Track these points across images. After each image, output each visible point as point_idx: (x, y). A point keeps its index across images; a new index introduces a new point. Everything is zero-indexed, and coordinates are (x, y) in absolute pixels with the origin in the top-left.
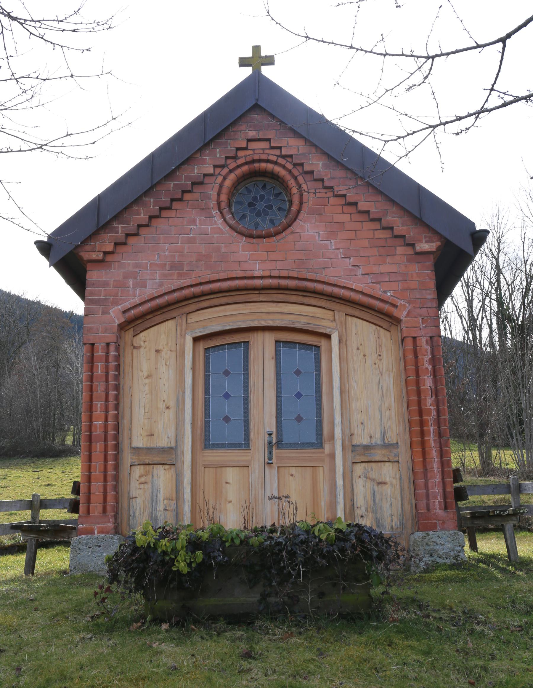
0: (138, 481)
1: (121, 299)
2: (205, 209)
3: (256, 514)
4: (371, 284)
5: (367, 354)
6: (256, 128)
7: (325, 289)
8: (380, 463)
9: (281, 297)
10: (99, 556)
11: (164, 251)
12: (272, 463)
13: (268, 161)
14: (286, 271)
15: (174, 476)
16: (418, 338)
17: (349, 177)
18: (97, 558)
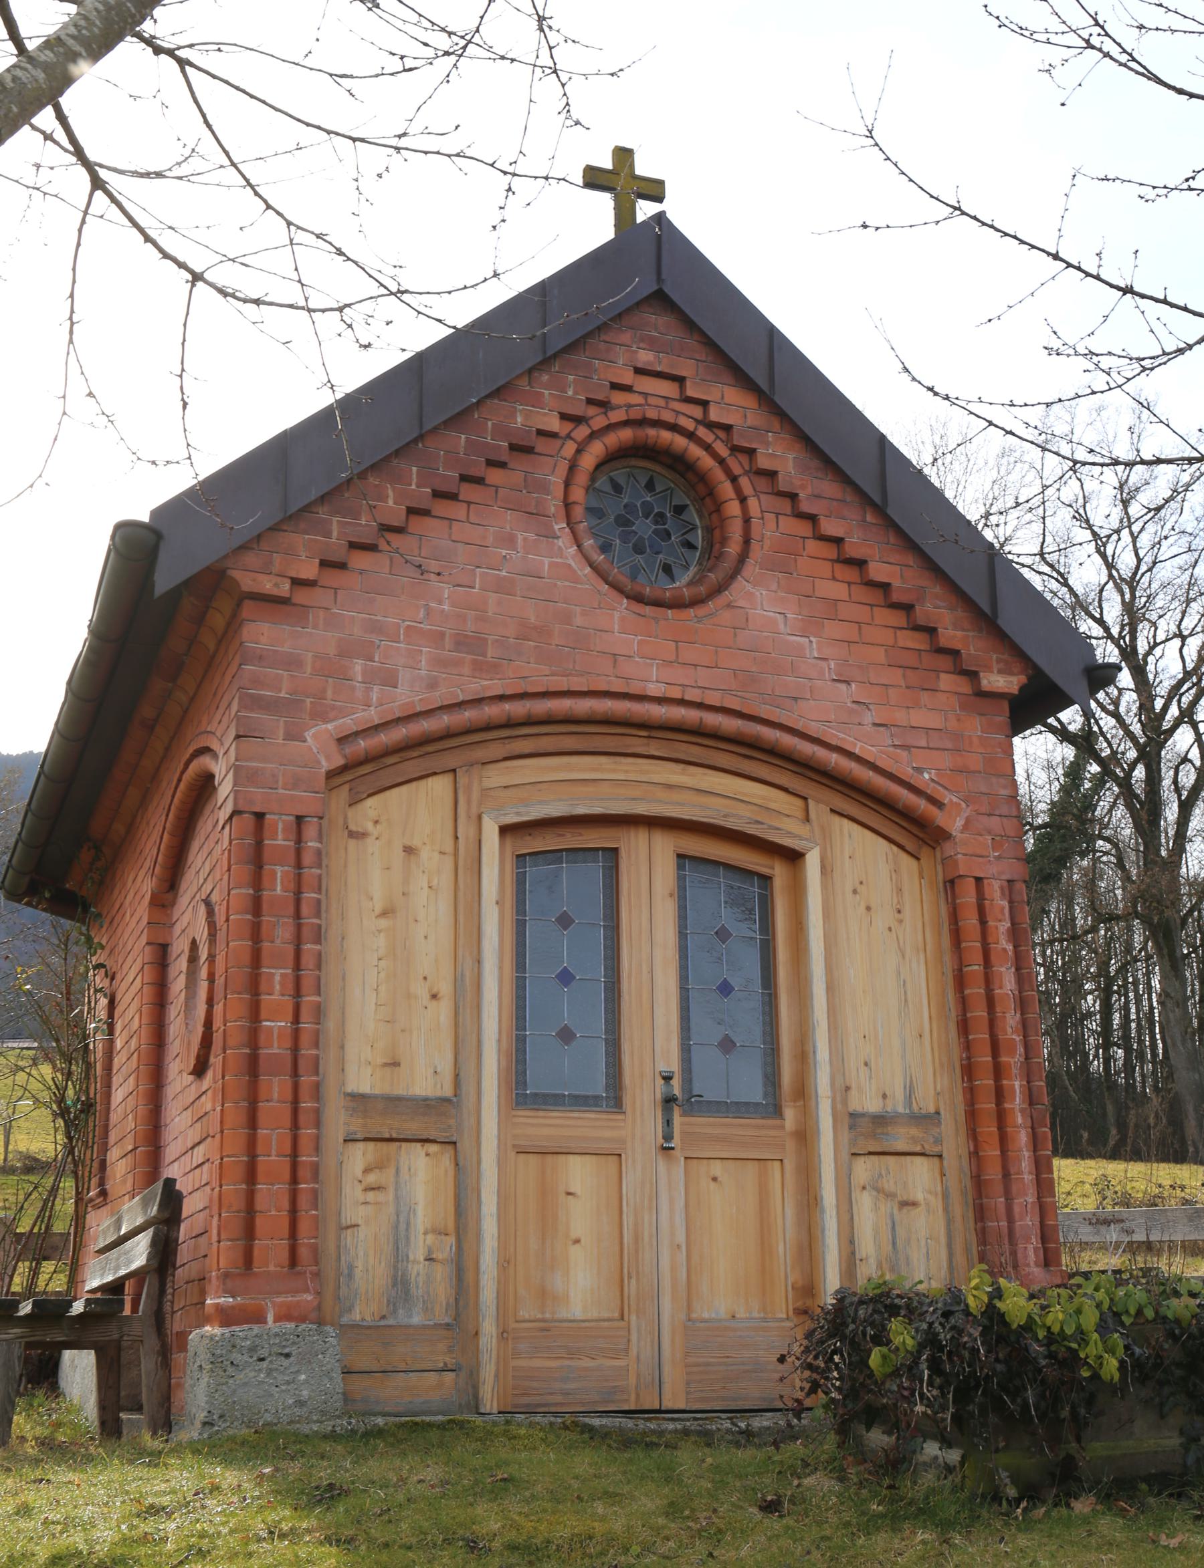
0: (360, 1181)
1: (333, 708)
2: (536, 514)
3: (638, 1273)
4: (891, 749)
5: (873, 905)
6: (652, 344)
7: (798, 747)
8: (903, 1158)
9: (695, 752)
10: (288, 1383)
11: (440, 602)
12: (672, 1148)
13: (674, 428)
14: (718, 694)
15: (451, 1173)
16: (986, 881)
17: (848, 499)
18: (283, 1388)
